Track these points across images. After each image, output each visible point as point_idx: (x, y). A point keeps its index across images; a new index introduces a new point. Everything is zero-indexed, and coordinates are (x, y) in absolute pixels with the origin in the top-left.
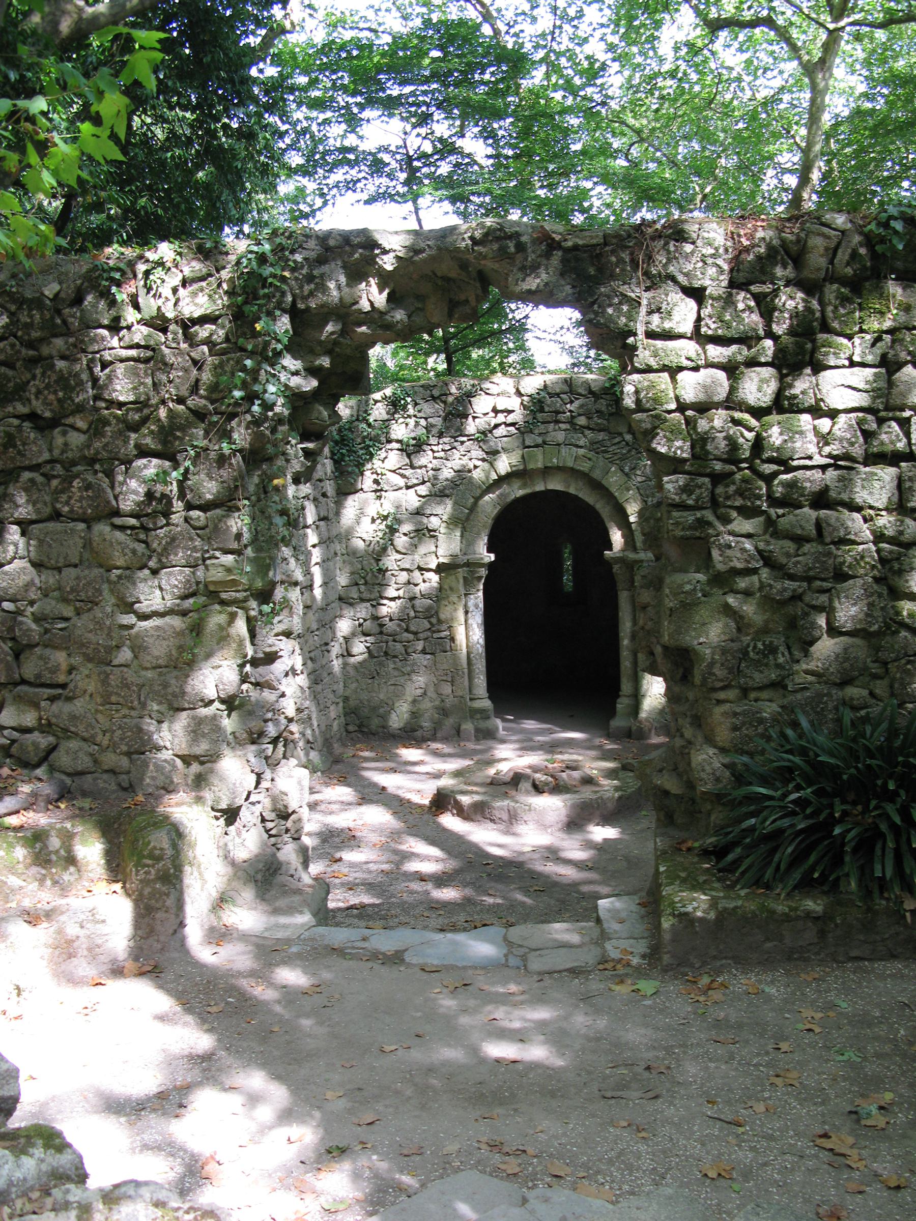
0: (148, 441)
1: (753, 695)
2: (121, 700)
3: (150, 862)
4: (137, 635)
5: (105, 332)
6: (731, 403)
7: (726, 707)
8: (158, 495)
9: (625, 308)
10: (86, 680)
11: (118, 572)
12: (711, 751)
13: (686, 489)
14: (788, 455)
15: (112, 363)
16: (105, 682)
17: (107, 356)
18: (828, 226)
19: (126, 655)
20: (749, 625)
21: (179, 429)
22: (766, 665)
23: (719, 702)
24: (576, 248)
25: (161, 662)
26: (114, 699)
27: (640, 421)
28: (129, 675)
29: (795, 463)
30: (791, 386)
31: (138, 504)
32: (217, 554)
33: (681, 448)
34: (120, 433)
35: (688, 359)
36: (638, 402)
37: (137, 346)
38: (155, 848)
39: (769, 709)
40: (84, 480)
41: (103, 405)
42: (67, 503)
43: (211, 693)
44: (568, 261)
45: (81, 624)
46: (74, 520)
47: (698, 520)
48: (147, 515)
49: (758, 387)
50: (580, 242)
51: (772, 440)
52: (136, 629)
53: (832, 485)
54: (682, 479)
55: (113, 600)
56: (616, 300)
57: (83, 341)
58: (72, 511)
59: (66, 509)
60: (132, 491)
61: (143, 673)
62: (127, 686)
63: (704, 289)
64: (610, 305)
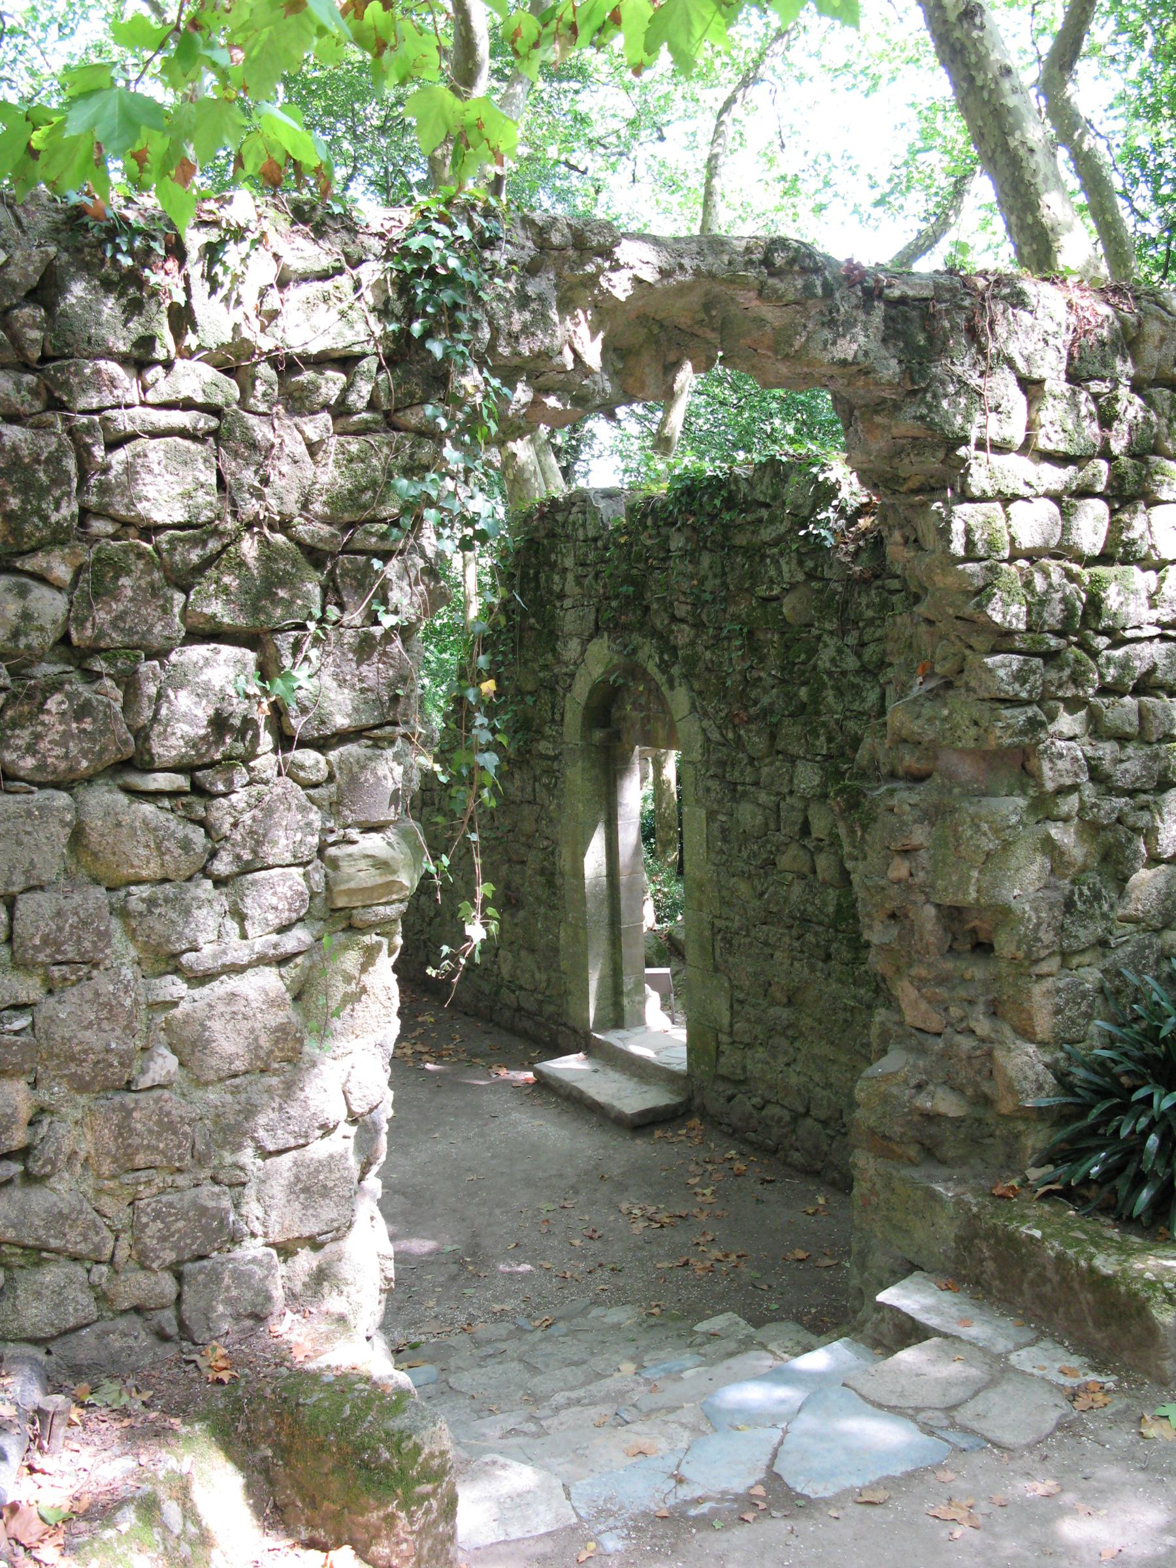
0: (215, 607)
1: (1075, 961)
2: (158, 1159)
3: (428, 1488)
4: (188, 1019)
5: (111, 368)
6: (1064, 551)
7: (1048, 984)
8: (236, 722)
9: (963, 401)
10: (77, 1132)
11: (144, 891)
12: (1031, 1049)
13: (1020, 677)
14: (1121, 622)
15: (133, 437)
16: (124, 1129)
17: (123, 420)
18: (1164, 308)
19: (165, 1064)
20: (1070, 864)
21: (282, 583)
22: (1092, 917)
23: (1040, 977)
24: (903, 300)
25: (239, 1065)
26: (140, 1159)
27: (972, 575)
28: (172, 1102)
29: (1129, 634)
30: (1129, 527)
31: (193, 743)
32: (354, 833)
33: (1016, 616)
34: (154, 590)
35: (1027, 484)
36: (970, 544)
37: (187, 405)
38: (432, 1455)
39: (1091, 977)
40: (70, 697)
41: (110, 528)
42: (31, 749)
43: (336, 1112)
44: (892, 319)
45: (68, 1013)
46: (42, 786)
47: (1029, 719)
48: (212, 765)
49: (1091, 525)
50: (910, 293)
51: (1109, 602)
52: (184, 1006)
53: (1162, 662)
54: (1016, 661)
55: (133, 953)
56: (951, 389)
57: (65, 386)
58: (41, 767)
59: (30, 762)
60: (185, 718)
61: (198, 1094)
62: (171, 1127)
63: (1040, 382)
64: (946, 396)
